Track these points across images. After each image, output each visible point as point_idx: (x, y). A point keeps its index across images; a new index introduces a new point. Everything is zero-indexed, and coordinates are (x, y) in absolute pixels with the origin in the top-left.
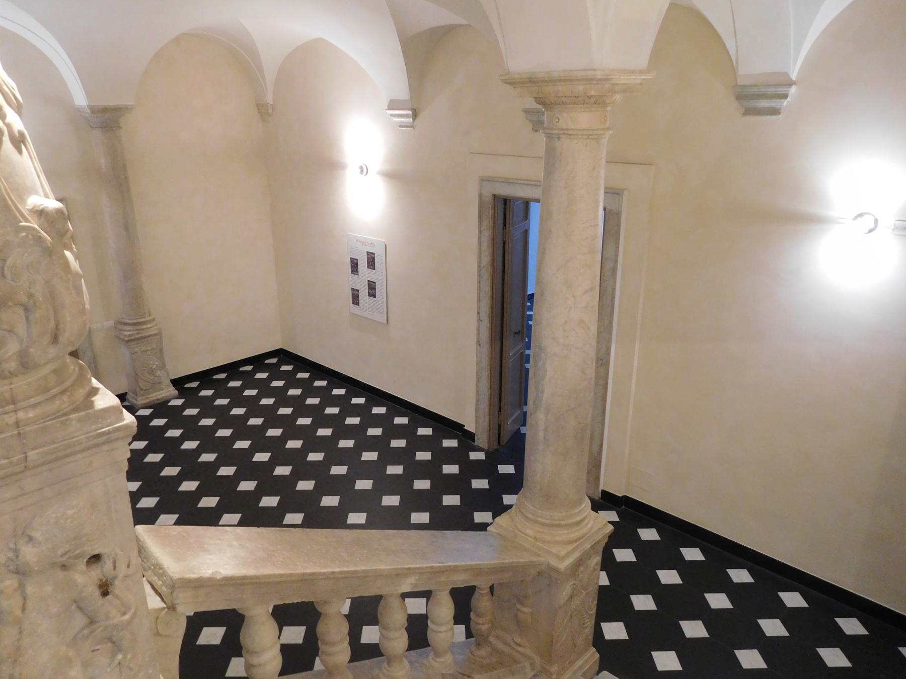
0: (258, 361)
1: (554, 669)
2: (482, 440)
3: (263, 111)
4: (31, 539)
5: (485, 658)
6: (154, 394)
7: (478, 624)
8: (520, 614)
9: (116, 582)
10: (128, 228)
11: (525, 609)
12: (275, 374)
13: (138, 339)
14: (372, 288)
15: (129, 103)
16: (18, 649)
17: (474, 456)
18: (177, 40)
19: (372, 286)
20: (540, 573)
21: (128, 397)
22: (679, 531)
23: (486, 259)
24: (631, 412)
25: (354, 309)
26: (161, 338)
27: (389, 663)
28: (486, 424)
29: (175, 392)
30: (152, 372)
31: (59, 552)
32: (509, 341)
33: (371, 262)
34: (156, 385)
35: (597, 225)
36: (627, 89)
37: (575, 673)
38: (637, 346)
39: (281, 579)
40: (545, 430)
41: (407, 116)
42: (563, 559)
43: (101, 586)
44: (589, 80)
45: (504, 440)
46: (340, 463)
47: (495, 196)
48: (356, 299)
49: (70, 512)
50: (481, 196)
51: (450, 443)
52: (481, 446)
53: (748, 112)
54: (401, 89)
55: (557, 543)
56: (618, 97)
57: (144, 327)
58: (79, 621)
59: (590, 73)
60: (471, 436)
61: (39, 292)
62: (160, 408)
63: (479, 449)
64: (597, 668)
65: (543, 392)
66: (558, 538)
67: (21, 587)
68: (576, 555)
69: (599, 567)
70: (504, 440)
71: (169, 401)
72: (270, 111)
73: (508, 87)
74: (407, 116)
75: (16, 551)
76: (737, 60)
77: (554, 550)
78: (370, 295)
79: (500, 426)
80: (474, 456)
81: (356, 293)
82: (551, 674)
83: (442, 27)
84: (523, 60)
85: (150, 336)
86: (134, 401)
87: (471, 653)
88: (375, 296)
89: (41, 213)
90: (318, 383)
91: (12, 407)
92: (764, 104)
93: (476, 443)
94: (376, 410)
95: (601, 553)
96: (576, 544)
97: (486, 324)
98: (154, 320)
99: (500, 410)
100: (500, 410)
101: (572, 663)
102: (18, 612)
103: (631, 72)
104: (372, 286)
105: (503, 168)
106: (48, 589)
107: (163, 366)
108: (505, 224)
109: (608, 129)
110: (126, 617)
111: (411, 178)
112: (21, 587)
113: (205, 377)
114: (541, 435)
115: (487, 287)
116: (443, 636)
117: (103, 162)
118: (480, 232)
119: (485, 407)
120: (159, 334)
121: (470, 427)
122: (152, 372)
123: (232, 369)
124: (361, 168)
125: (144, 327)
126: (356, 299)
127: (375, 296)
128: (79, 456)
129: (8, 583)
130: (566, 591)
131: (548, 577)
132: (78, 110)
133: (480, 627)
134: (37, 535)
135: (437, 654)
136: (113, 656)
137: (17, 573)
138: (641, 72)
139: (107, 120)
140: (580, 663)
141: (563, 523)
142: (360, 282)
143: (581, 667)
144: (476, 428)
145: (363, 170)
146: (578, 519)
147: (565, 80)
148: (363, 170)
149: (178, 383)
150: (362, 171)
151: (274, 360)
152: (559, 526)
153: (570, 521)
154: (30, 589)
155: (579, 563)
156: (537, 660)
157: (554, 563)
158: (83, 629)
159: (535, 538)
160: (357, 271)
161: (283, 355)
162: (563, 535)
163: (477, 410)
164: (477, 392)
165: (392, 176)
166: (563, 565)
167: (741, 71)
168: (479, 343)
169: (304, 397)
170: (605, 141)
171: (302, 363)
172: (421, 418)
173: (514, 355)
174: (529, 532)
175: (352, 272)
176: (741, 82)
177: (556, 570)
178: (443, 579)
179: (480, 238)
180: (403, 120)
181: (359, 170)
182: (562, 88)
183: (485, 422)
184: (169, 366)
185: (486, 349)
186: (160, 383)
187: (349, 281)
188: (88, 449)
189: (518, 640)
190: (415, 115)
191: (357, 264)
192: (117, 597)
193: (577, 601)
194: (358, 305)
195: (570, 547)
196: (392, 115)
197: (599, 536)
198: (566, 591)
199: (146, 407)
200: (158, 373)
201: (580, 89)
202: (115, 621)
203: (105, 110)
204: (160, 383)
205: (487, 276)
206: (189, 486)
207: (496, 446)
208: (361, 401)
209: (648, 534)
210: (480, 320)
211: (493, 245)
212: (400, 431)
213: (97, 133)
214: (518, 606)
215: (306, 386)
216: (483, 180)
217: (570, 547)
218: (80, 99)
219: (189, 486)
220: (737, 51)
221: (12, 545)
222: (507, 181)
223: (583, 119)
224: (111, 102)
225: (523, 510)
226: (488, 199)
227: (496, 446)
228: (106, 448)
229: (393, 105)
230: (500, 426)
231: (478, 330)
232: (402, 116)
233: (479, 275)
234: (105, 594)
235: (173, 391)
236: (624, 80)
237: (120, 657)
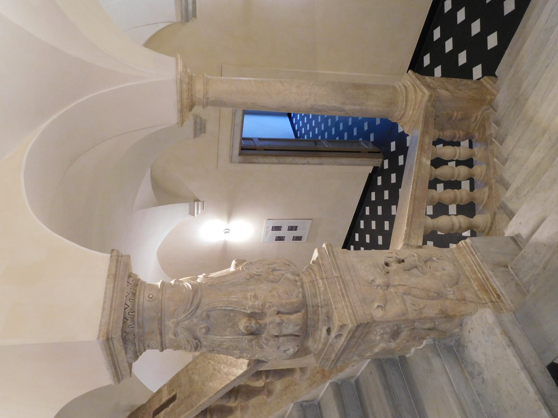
1: (489, 97)
2: (377, 162)
4: (373, 281)
5: (479, 133)
7: (459, 137)
8: (458, 118)
9: (398, 257)
11: (455, 114)
14: (292, 228)
16: (423, 289)
17: (386, 166)
19: (291, 228)
20: (433, 106)
22: (425, 43)
23: (274, 159)
24: (357, 74)
27: (474, 176)
28: (368, 159)
31: (380, 271)
32: (320, 147)
33: (277, 228)
35: (250, 80)
36: (185, 66)
37: (493, 88)
38: (319, 72)
39: (412, 207)
40: (354, 105)
41: (198, 205)
42: (423, 93)
43: (400, 263)
44: (181, 81)
45: (377, 150)
47: (240, 154)
48: (298, 238)
49: (363, 268)
50: (240, 162)
52: (380, 163)
53: (194, 15)
54: (184, 207)
55: (416, 98)
56: (188, 70)
58: (415, 271)
59: (178, 81)
60: (375, 169)
61: (266, 266)
63: (383, 163)
64: (493, 78)
65: (335, 107)
66: (414, 98)
67: (394, 286)
68: (423, 87)
69: (432, 77)
70: (377, 150)
73: (185, 123)
74: (198, 205)
75: (378, 286)
76: (169, 22)
77: (419, 98)
78: (296, 230)
79: (369, 152)
80: (386, 166)
82: (491, 99)
83: (152, 185)
84: (171, 115)
87: (477, 141)
88: (297, 227)
89: (237, 265)
91: (315, 282)
92: (190, 7)
93: (379, 166)
95: (424, 77)
96: (417, 88)
97: (310, 160)
99: (360, 152)
100: (360, 152)
101: (487, 89)
102: (405, 287)
103: (177, 64)
104: (291, 228)
105: (225, 149)
106: (397, 278)
108: (255, 150)
109: (203, 75)
110: (415, 255)
111: (231, 204)
112: (394, 286)
114: (357, 107)
115: (289, 159)
116: (462, 151)
118: (259, 163)
119: (358, 161)
121: (370, 169)
124: (225, 232)
126: (298, 238)
127: (297, 227)
128: (338, 262)
129: (392, 290)
130: (443, 92)
131: (434, 100)
133: (461, 136)
134: (371, 278)
135: (474, 154)
136: (433, 261)
137: (388, 287)
138: (177, 60)
140: (488, 86)
141: (405, 95)
143: (491, 85)
144: (368, 165)
145: (227, 231)
146: (403, 87)
147: (181, 94)
148: (227, 231)
150: (228, 232)
152: (407, 97)
153: (404, 91)
154: (396, 283)
155: (428, 86)
156: (484, 107)
157: (426, 98)
158: (419, 271)
159: (414, 110)
162: (411, 96)
163: (359, 165)
164: (349, 165)
165: (230, 214)
166: (427, 93)
167: (174, 20)
168: (321, 164)
170: (209, 77)
173: (327, 144)
174: (411, 113)
175: (283, 240)
176: (180, 20)
177: (431, 96)
178: (426, 147)
179: (263, 163)
180: (200, 208)
182: (185, 96)
183: (367, 160)
185: (324, 160)
187: (289, 242)
188: (335, 258)
189: (473, 119)
190: (197, 200)
191: (279, 237)
192: (406, 258)
193: (451, 87)
194: (301, 237)
195: (418, 90)
196: (197, 214)
197: (413, 76)
198: (443, 92)
201: (185, 87)
202: (417, 260)
205: (283, 159)
207: (381, 155)
210: (308, 163)
211: (266, 155)
212: (368, 225)
214: (454, 119)
216: (231, 161)
217: (418, 90)
220: (164, 22)
221: (375, 287)
222: (232, 147)
223: (199, 87)
225: (399, 118)
226: (241, 158)
227: (381, 155)
228: (335, 254)
229: (192, 213)
230: (369, 152)
231: (314, 164)
232: (198, 208)
233: (283, 164)
234: (403, 261)
236: (180, 67)
237: (434, 258)
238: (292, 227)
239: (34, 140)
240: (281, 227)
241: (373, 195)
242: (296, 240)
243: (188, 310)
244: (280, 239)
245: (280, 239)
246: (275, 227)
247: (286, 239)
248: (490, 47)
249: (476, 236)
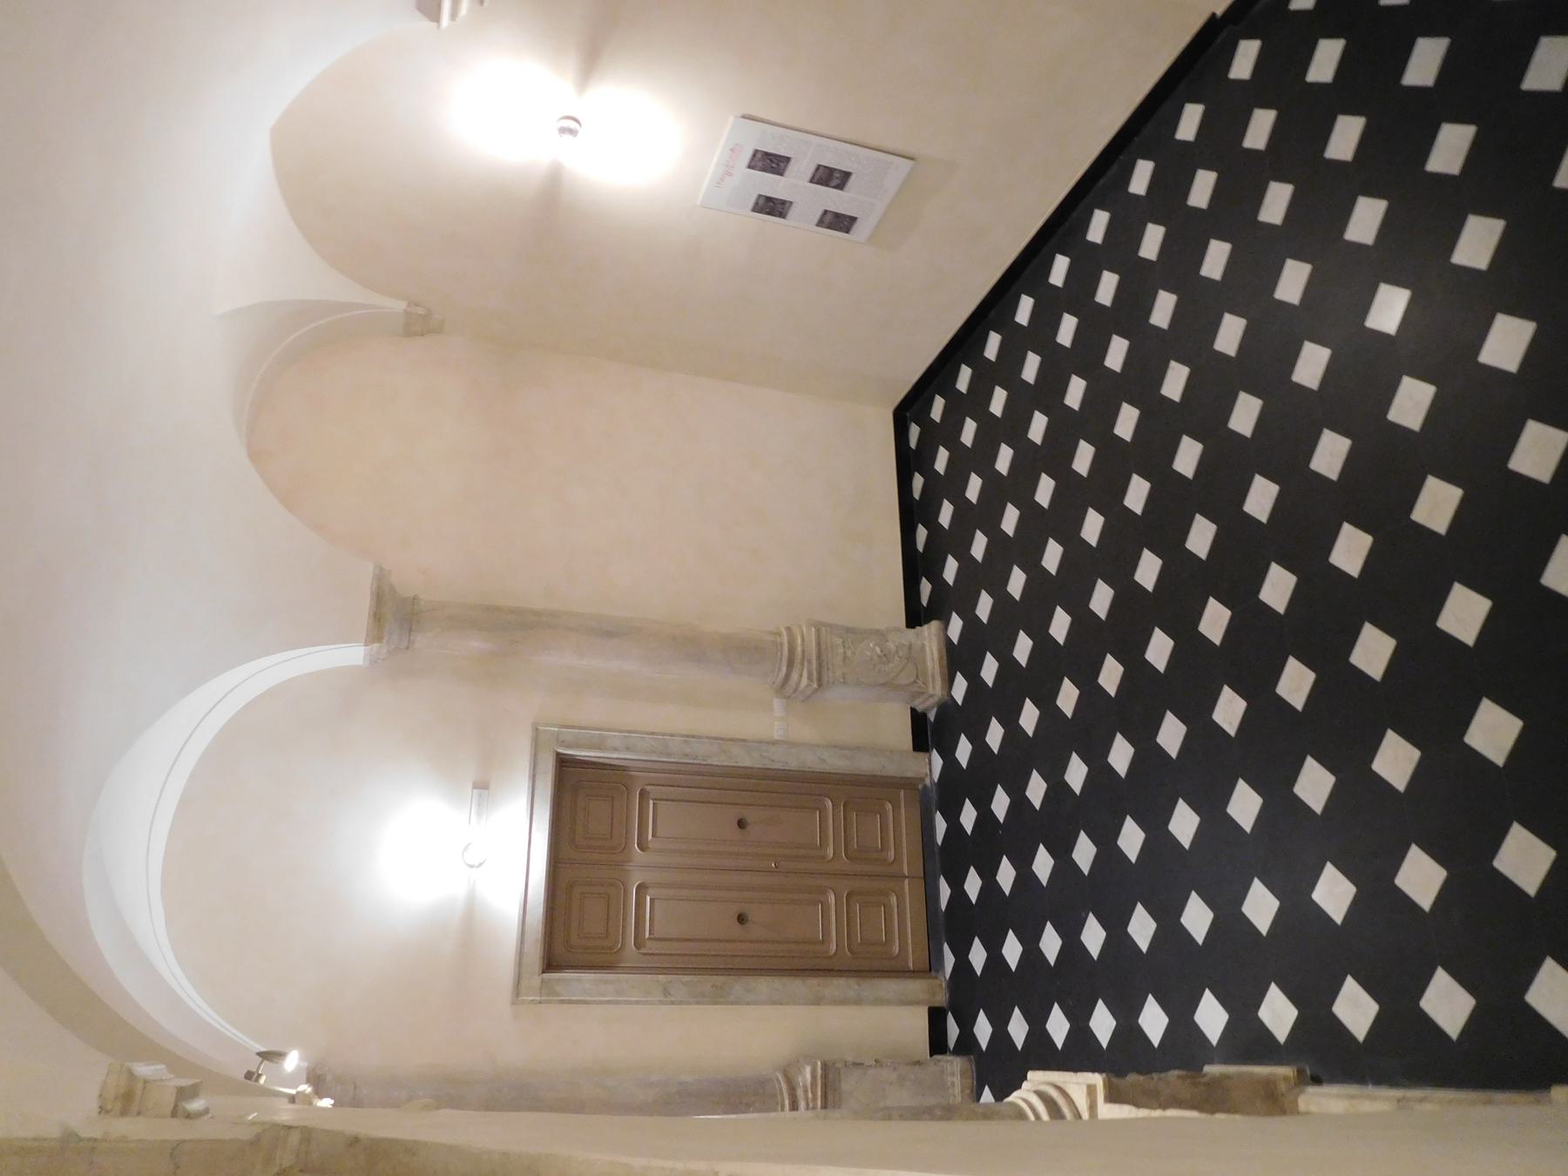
0: (908, 462)
3: (419, 325)
6: (929, 664)
10: (608, 631)
12: (948, 432)
13: (820, 666)
15: (369, 569)
18: (256, 455)
21: (920, 708)
25: (861, 231)
26: (823, 624)
29: (934, 626)
30: (886, 656)
33: (772, 163)
34: (913, 656)
46: (1049, 432)
48: (840, 222)
51: (1141, 178)
57: (799, 649)
62: (961, 658)
71: (948, 641)
72: (421, 311)
78: (840, 187)
81: (828, 218)
85: (819, 644)
86: (932, 701)
88: (847, 175)
90: (963, 384)
94: (963, 384)
98: (788, 629)
104: (829, 177)
107: (881, 635)
113: (916, 566)
117: (476, 644)
120: (818, 626)
122: (886, 656)
123: (912, 513)
124: (563, 130)
125: (799, 649)
126: (840, 222)
127: (847, 175)
132: (373, 661)
139: (396, 616)
142: (811, 201)
149: (915, 616)
150: (572, 132)
151: (914, 431)
160: (783, 202)
161: (909, 410)
169: (984, 417)
171: (937, 376)
172: (1115, 168)
175: (782, 215)
181: (567, 137)
184: (882, 626)
186: (910, 647)
187: (800, 224)
191: (769, 199)
194: (853, 219)
196: (454, 15)
199: (950, 681)
200: (891, 646)
203: (377, 617)
204: (910, 647)
206: (1023, 648)
208: (965, 374)
209: (1245, 60)
212: (1082, 279)
213: (421, 640)
215: (959, 407)
218: (354, 654)
219: (1023, 648)
224: (365, 603)
235: (931, 630)
238: (831, 171)
239: (715, 160)
240: (788, 159)
241: (1061, 265)
242: (829, 227)
243: (814, 1099)
244: (772, 207)
245: (772, 207)
246: (767, 154)
247: (793, 213)
248: (1350, 986)
249: (602, 960)
